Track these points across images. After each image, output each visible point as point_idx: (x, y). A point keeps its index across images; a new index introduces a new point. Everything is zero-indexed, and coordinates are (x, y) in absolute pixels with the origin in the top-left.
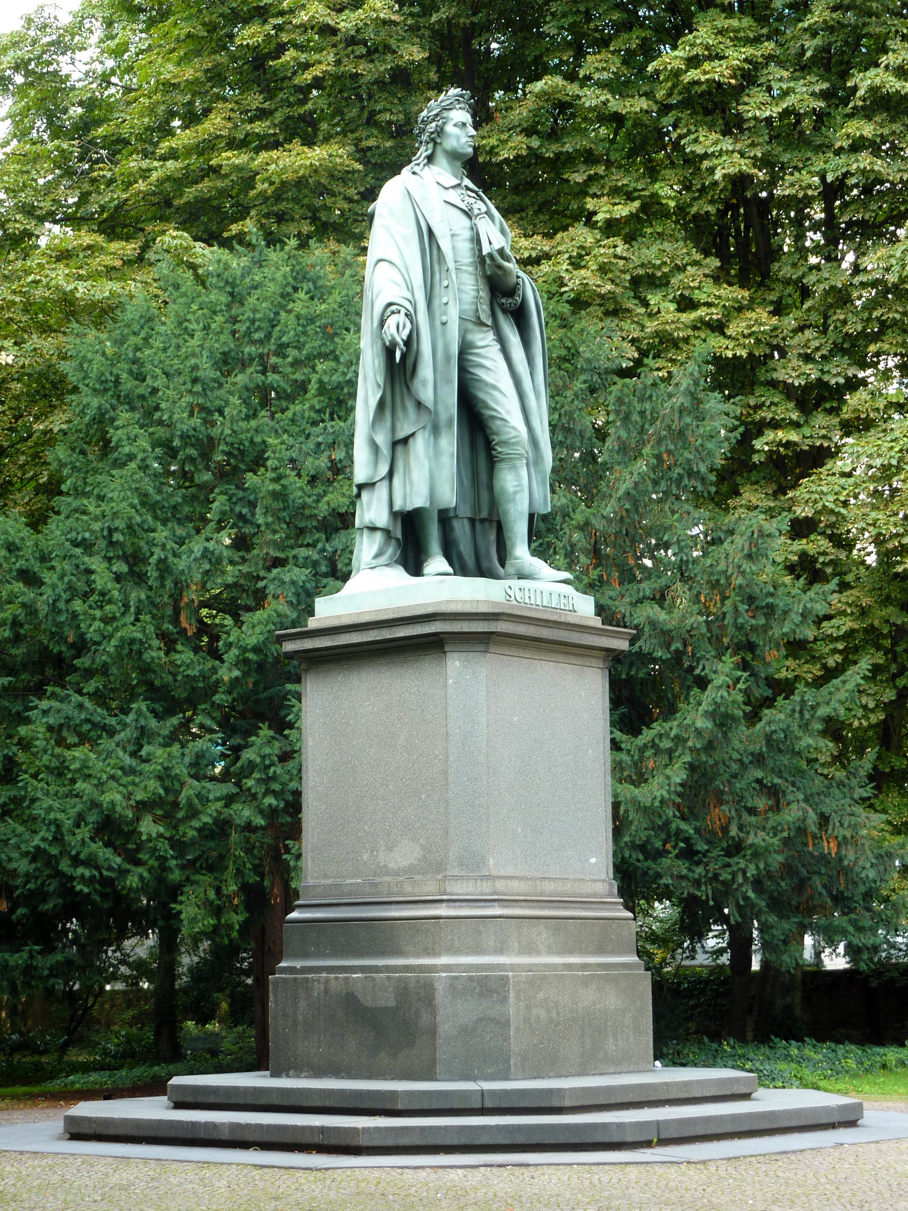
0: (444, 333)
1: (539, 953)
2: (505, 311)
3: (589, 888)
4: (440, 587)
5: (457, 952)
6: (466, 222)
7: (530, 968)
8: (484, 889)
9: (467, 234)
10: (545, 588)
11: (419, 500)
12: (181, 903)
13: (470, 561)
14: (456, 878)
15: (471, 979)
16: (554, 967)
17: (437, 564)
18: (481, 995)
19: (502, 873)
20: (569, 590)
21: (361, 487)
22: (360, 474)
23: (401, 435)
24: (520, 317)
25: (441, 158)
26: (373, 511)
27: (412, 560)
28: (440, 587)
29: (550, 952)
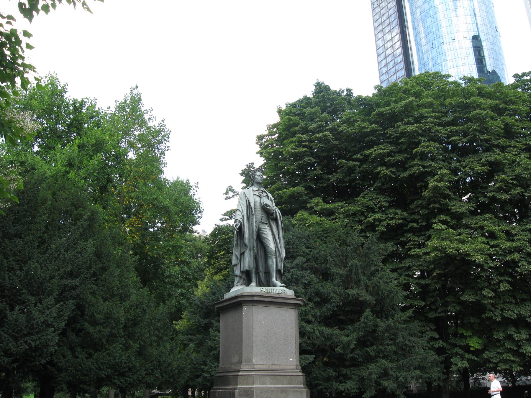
0: (252, 226)
1: (267, 384)
2: (272, 220)
3: (288, 367)
4: (254, 289)
5: (242, 384)
6: (259, 199)
7: (262, 388)
8: (251, 367)
9: (259, 201)
10: (279, 289)
11: (247, 268)
12: (331, 393)
13: (265, 283)
14: (245, 365)
15: (244, 391)
16: (271, 388)
17: (253, 284)
18: (246, 396)
19: (258, 363)
20: (285, 288)
21: (234, 265)
22: (234, 262)
23: (242, 252)
24: (276, 220)
25: (255, 184)
26: (237, 272)
27: (248, 283)
28: (254, 289)
29: (271, 384)
